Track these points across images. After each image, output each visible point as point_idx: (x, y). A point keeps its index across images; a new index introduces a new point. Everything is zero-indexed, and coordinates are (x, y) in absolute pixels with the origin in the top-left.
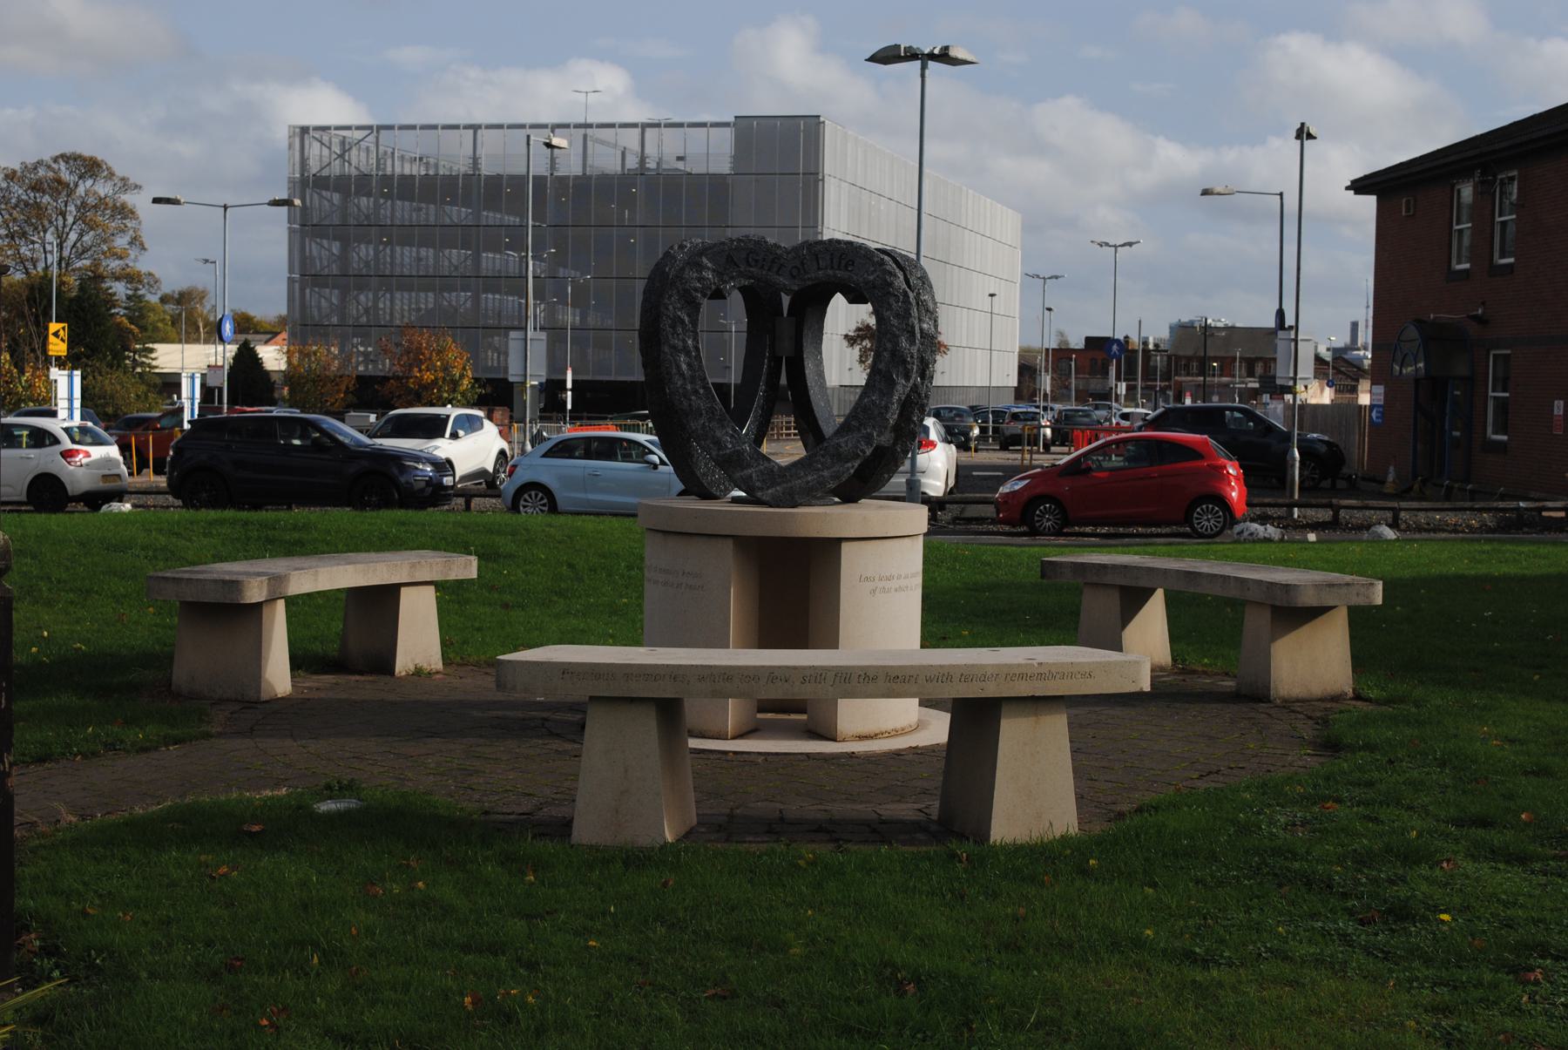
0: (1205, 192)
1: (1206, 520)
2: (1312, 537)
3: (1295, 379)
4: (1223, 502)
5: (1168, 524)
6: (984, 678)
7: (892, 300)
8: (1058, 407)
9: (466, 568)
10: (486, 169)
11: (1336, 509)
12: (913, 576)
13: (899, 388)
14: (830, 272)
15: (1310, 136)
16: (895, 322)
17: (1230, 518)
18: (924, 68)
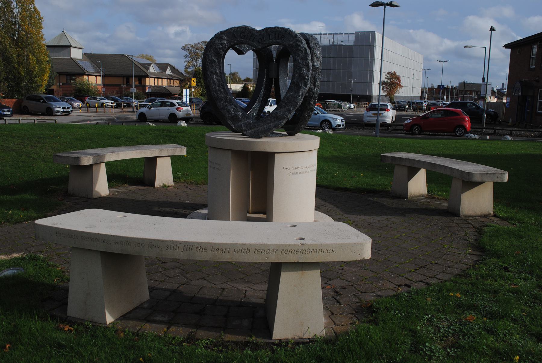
0: (465, 47)
1: (459, 132)
2: (488, 137)
3: (486, 95)
4: (464, 127)
5: (449, 132)
6: (269, 252)
7: (300, 52)
8: (429, 101)
9: (182, 151)
10: (335, 43)
11: (495, 130)
12: (311, 166)
13: (302, 90)
14: (274, 41)
15: (494, 30)
16: (300, 61)
17: (466, 131)
18: (385, 8)
